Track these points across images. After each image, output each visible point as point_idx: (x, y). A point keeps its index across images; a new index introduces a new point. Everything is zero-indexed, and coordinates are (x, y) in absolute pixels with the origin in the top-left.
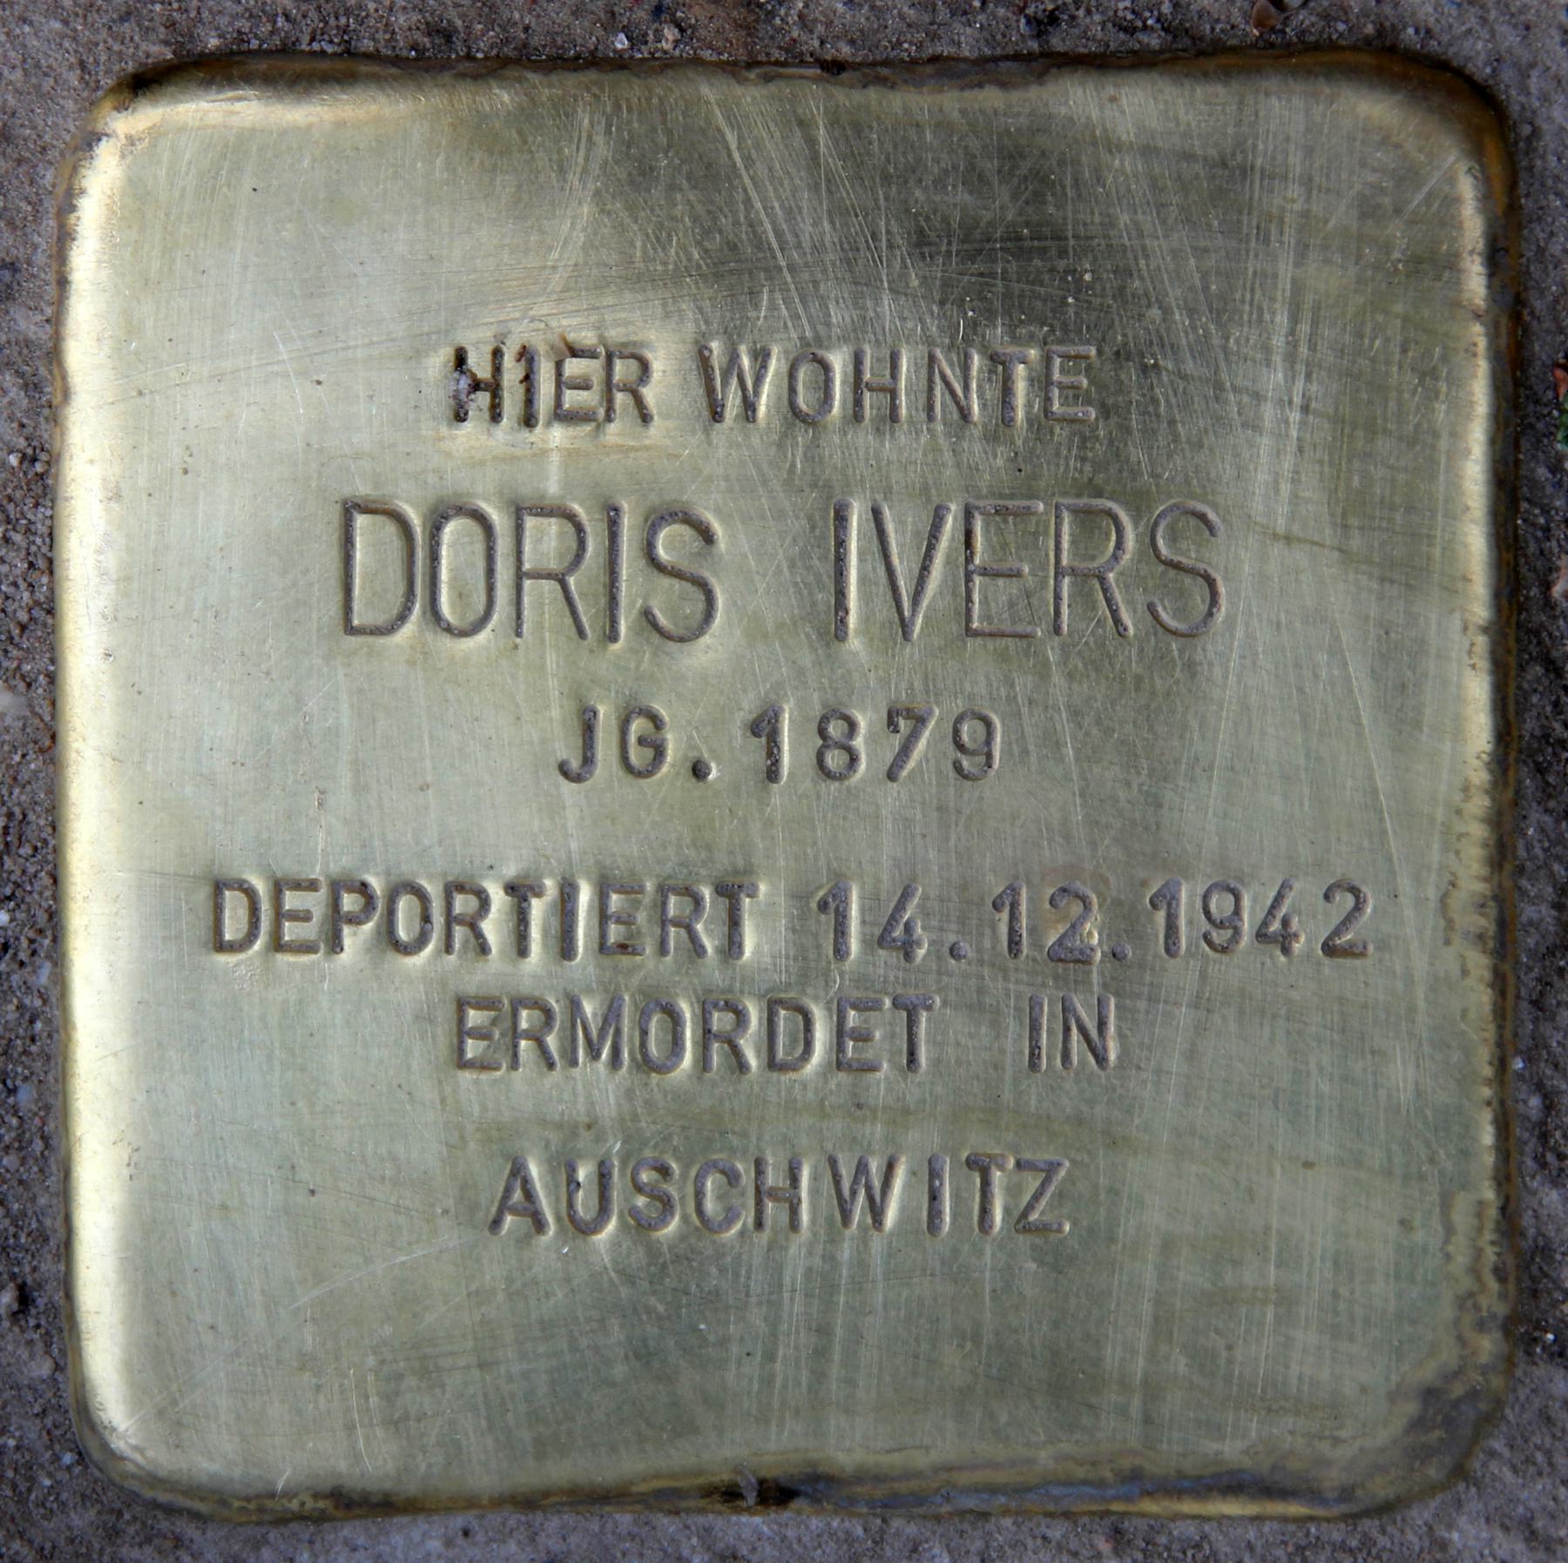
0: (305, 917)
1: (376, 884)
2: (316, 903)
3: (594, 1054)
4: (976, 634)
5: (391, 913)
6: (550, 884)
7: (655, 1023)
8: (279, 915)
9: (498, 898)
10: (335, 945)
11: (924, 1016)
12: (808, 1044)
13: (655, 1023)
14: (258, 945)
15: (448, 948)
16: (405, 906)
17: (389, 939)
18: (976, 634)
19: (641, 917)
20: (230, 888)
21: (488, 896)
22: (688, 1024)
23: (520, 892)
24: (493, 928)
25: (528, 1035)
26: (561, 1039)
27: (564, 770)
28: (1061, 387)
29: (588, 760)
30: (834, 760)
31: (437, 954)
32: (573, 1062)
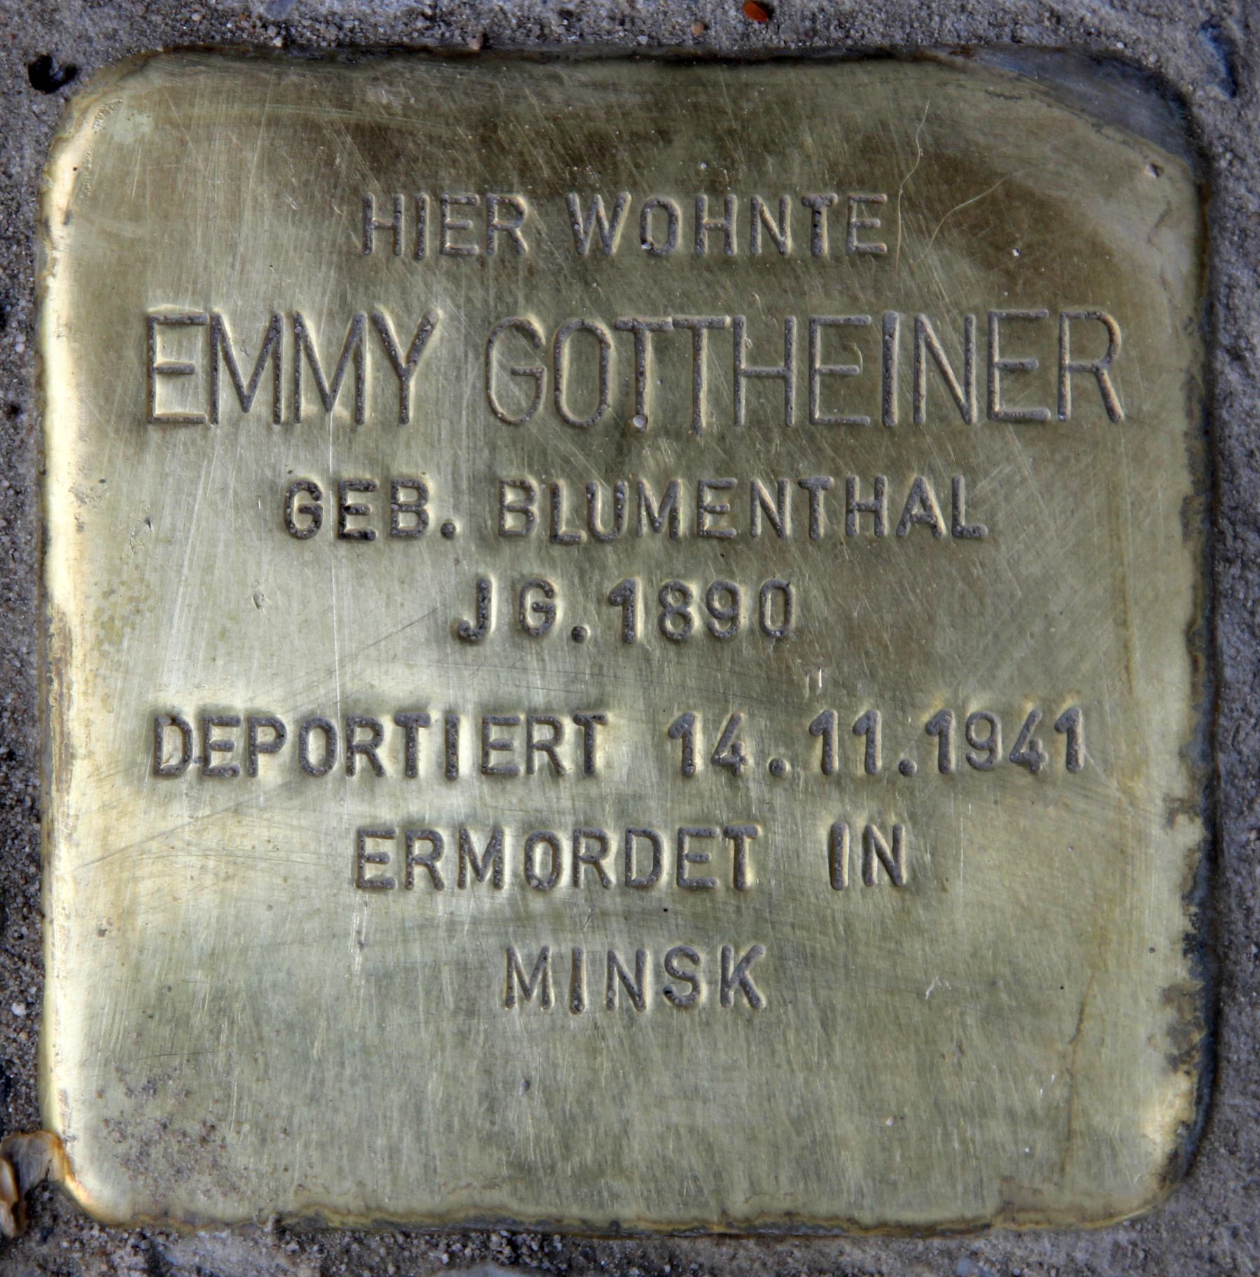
2: (236, 735)
6: (435, 715)
7: (539, 851)
8: (207, 747)
9: (389, 727)
10: (252, 771)
11: (747, 842)
12: (657, 862)
13: (539, 851)
21: (381, 726)
25: (421, 861)
28: (748, 376)
32: (461, 884)
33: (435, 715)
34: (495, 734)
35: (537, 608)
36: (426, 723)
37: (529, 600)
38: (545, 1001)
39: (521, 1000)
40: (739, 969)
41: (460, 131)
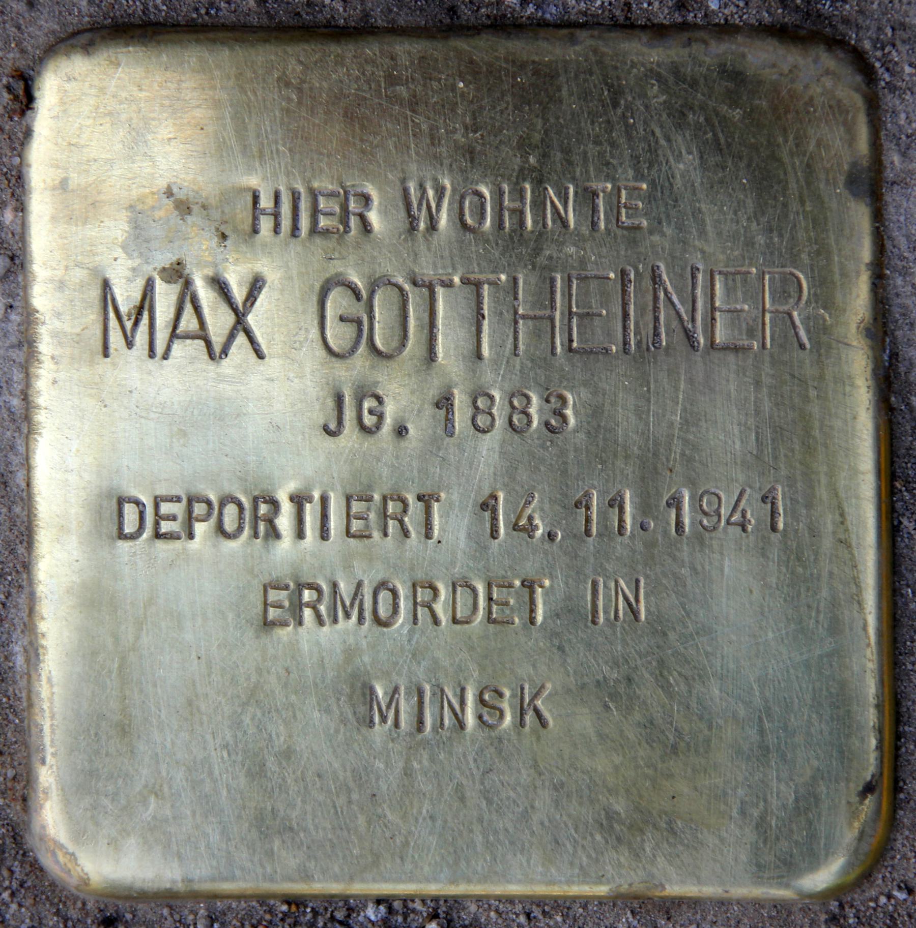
0: (174, 518)
1: (213, 497)
2: (177, 509)
3: (347, 615)
4: (495, 622)
5: (221, 514)
7: (384, 596)
9: (286, 507)
13: (384, 596)
14: (145, 536)
15: (256, 535)
16: (231, 511)
17: (220, 530)
18: (495, 622)
19: (372, 516)
20: (129, 502)
22: (402, 599)
23: (299, 501)
24: (285, 522)
26: (328, 609)
27: (326, 430)
29: (340, 422)
30: (481, 421)
31: (250, 538)
33: (316, 495)
34: (356, 507)
35: (371, 412)
36: (310, 500)
37: (366, 405)
38: (397, 724)
39: (380, 724)
40: (532, 700)
41: (318, 85)
